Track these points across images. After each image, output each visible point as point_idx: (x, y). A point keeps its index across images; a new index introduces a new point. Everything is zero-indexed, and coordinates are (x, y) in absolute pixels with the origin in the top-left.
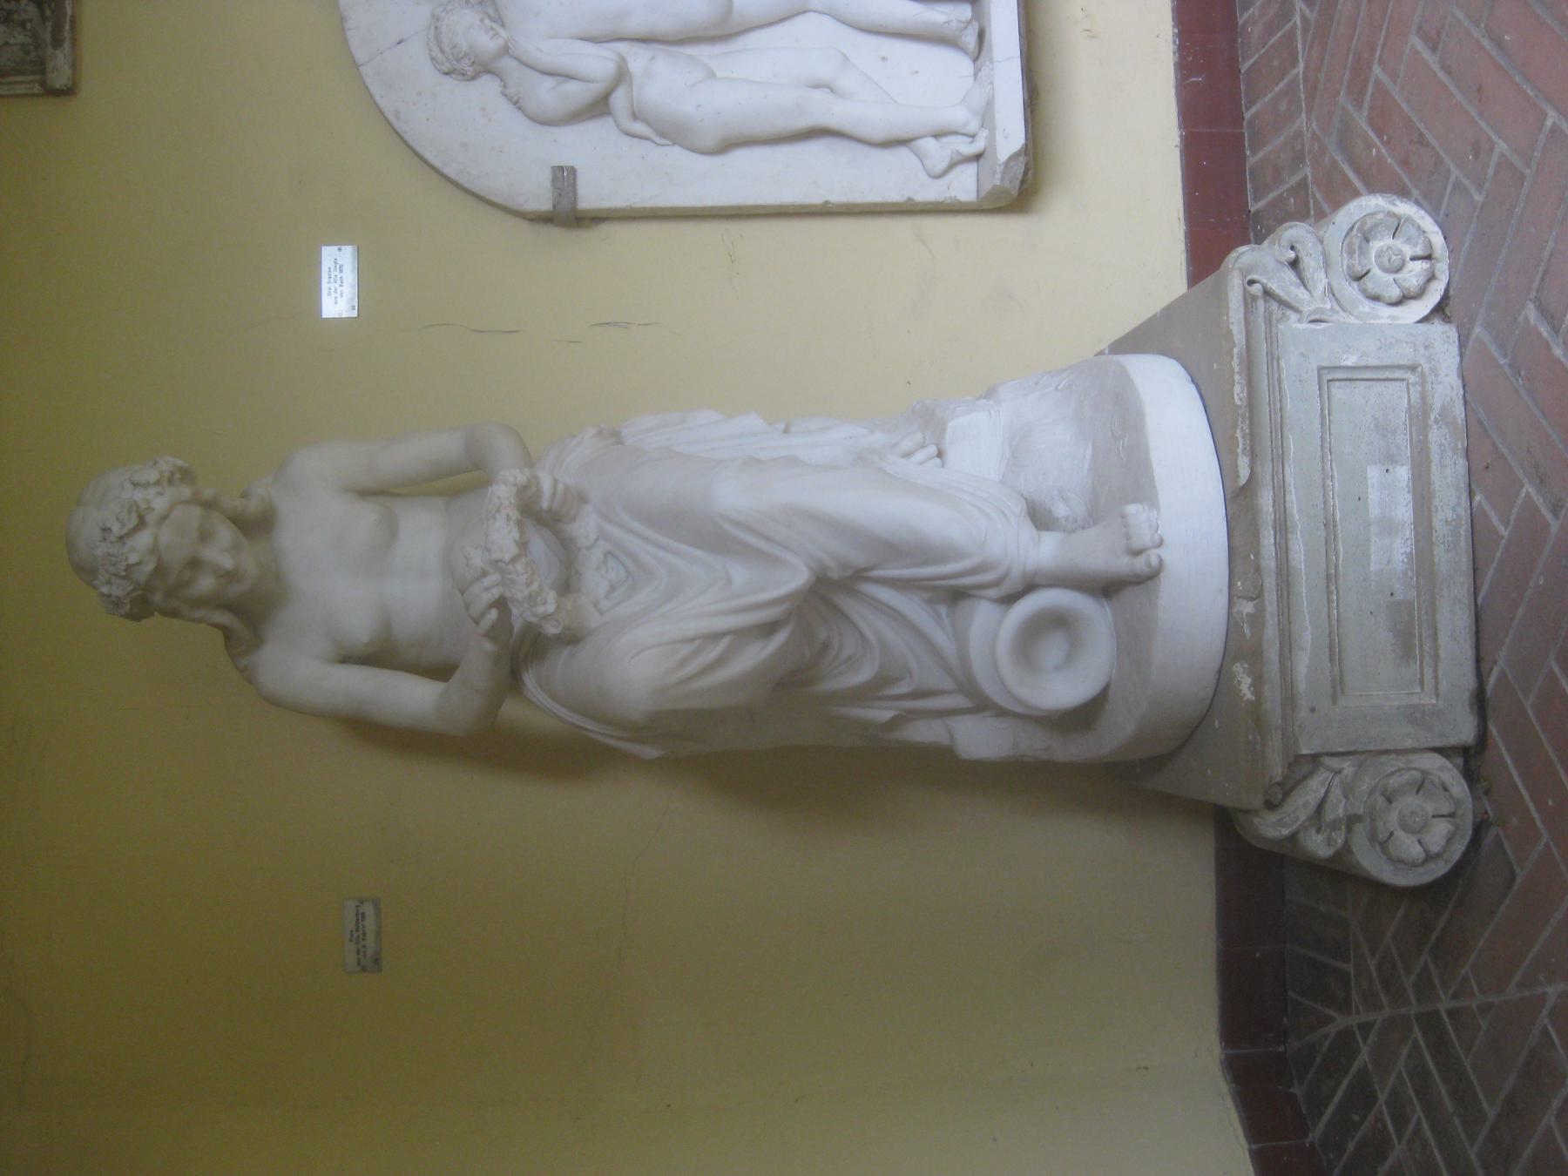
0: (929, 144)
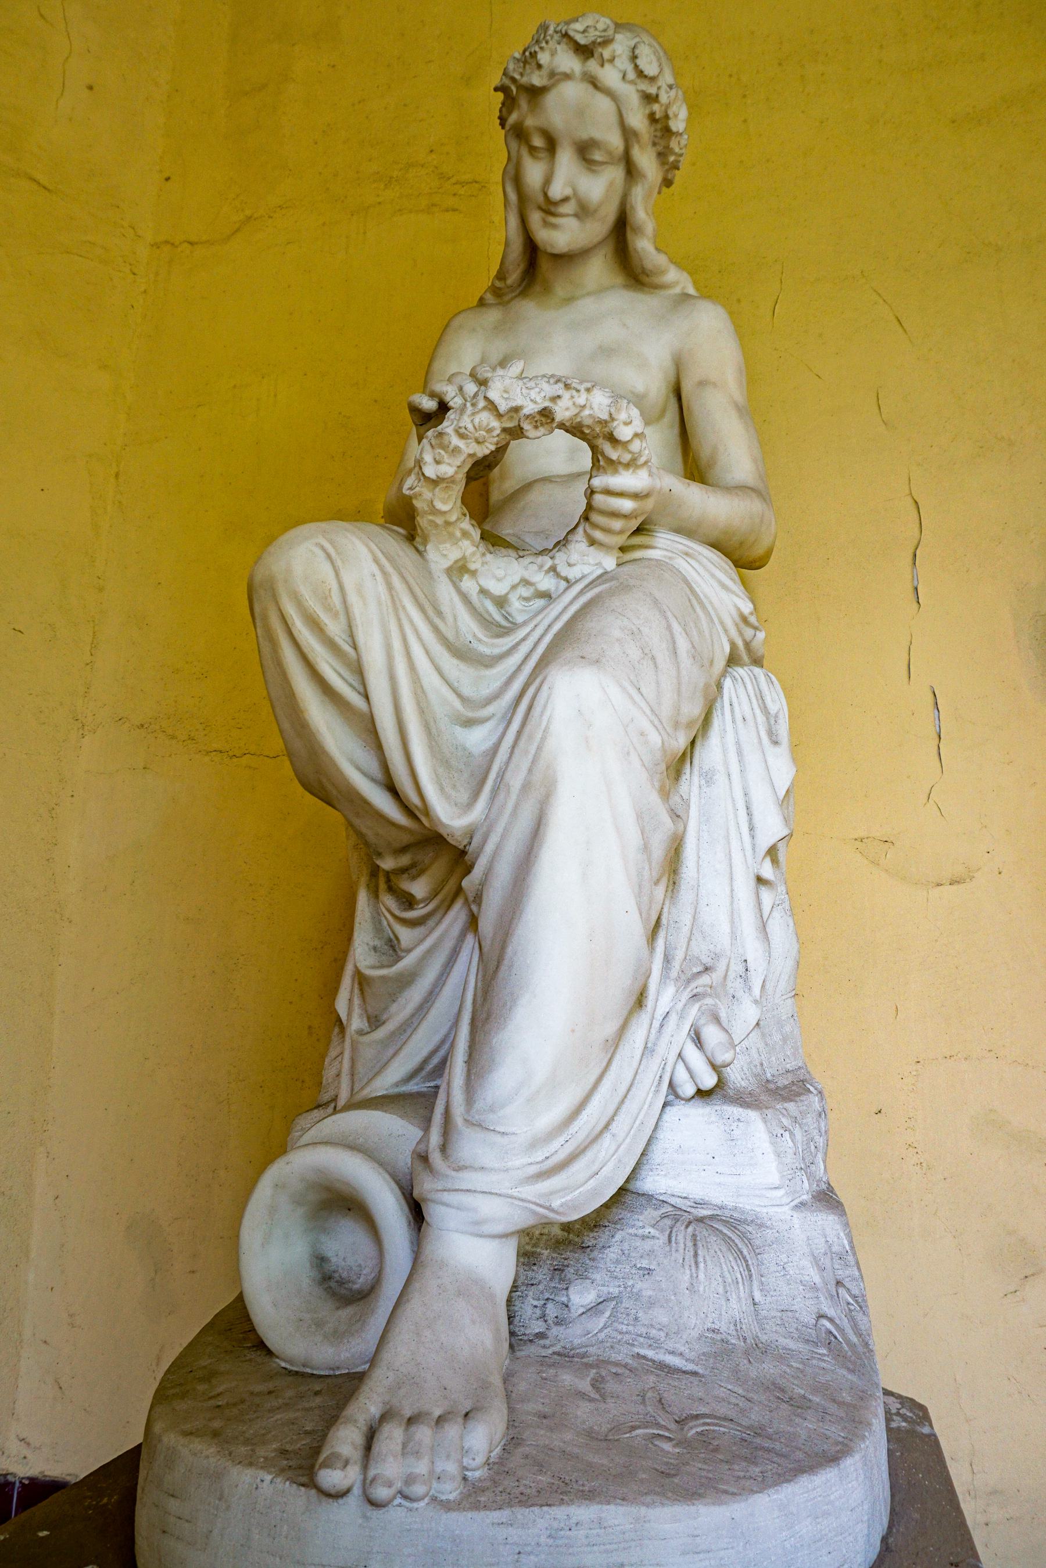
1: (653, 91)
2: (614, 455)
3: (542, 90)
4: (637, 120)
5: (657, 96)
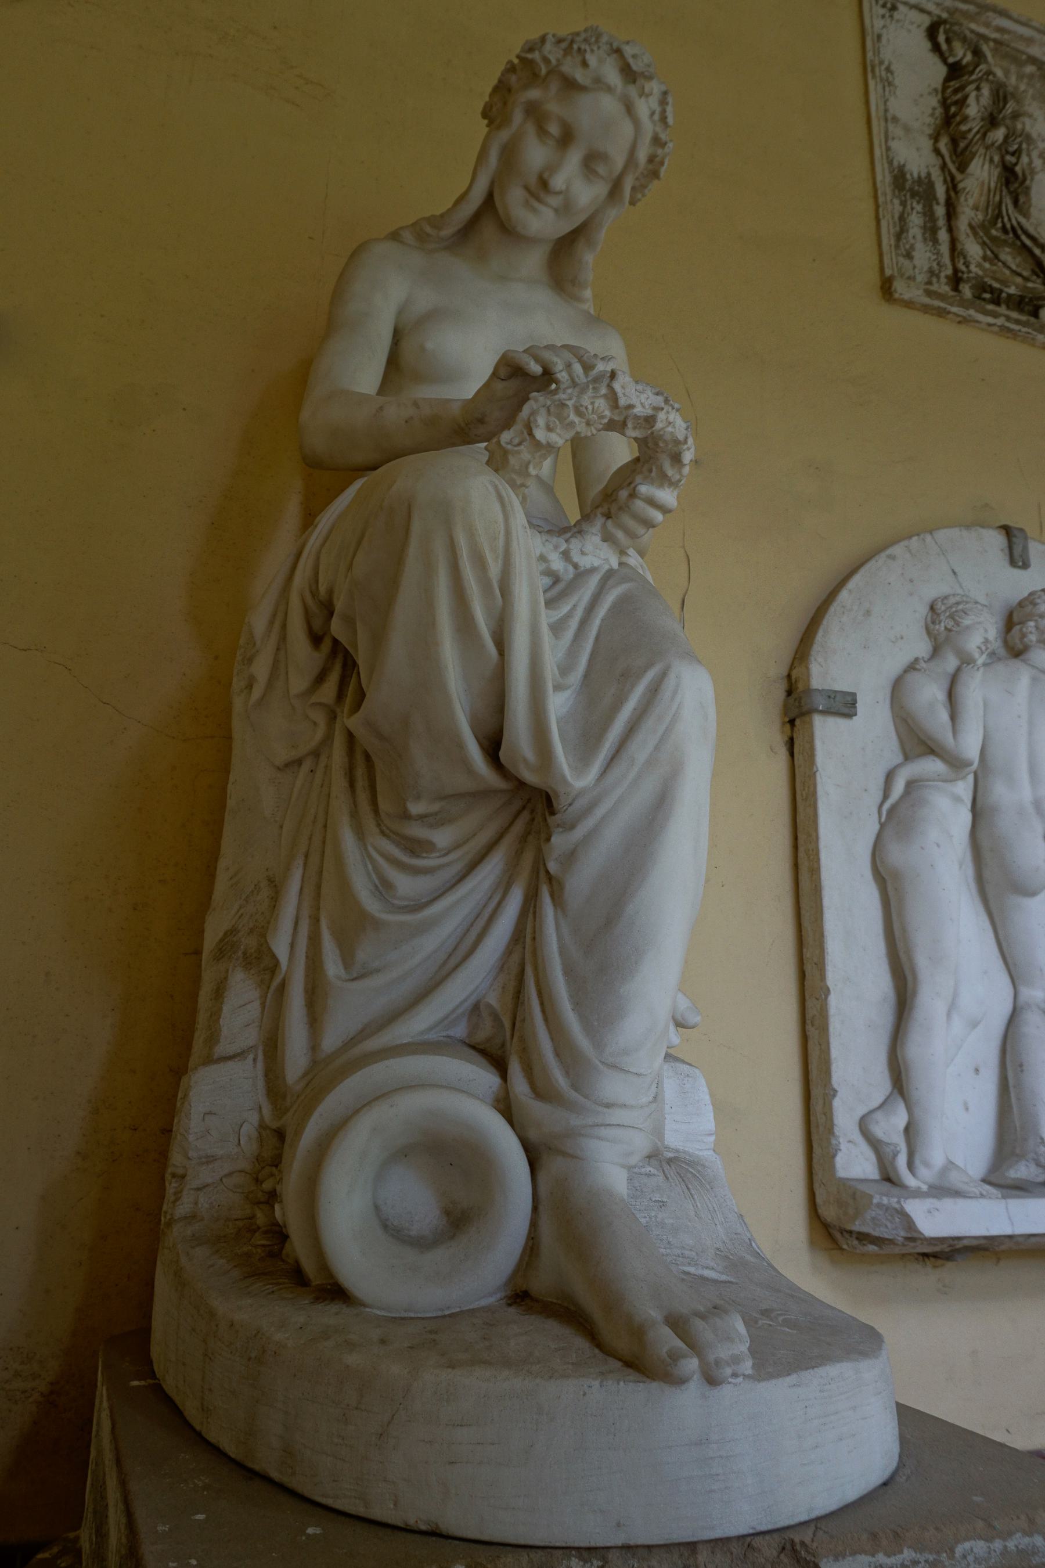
0: (900, 1118)
1: (663, 137)
2: (670, 472)
3: (583, 89)
4: (642, 155)
5: (666, 143)
